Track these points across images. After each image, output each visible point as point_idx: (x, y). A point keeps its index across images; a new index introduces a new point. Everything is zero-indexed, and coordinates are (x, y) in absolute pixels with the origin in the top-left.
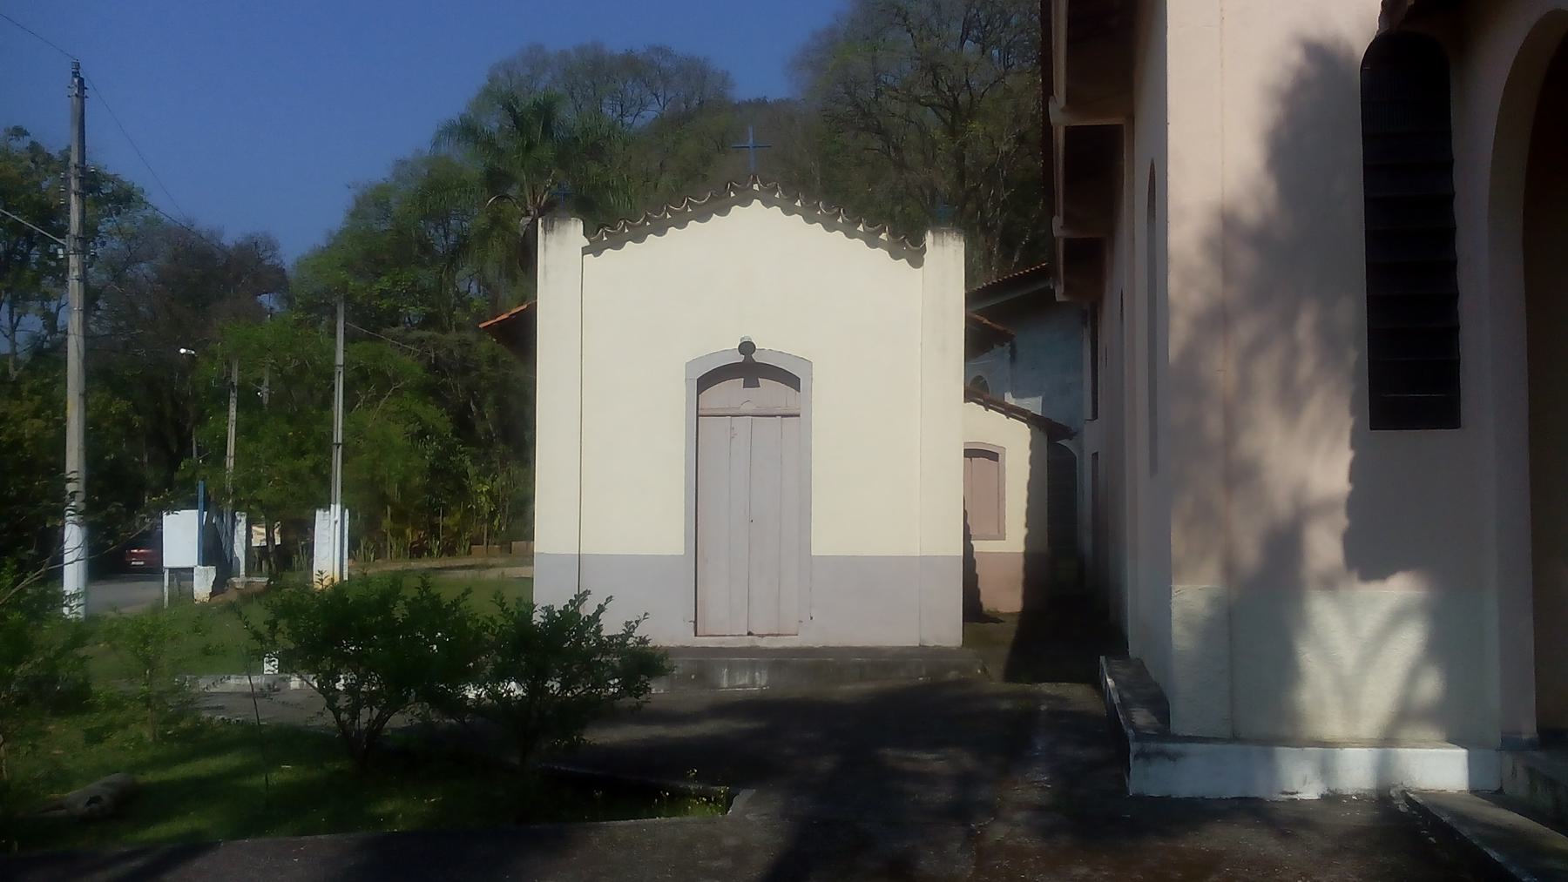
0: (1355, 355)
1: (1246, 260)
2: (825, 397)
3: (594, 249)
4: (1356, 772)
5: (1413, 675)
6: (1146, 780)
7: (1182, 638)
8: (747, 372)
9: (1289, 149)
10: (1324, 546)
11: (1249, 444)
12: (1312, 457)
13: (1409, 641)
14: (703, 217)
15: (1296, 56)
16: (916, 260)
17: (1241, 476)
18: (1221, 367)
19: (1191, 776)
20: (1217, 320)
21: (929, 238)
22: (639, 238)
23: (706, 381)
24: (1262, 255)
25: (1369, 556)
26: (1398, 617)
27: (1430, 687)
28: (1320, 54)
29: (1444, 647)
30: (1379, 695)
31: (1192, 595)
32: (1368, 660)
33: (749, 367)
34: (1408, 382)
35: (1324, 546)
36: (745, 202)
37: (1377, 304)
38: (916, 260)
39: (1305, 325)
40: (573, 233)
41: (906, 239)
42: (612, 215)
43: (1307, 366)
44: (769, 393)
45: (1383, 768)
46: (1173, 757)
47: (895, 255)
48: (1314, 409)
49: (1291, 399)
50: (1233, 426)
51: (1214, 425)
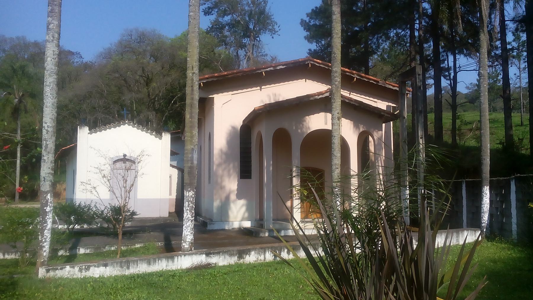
0: (238, 169)
1: (224, 156)
2: (142, 168)
3: (90, 133)
4: (236, 225)
5: (244, 214)
6: (209, 227)
7: (215, 210)
8: (126, 162)
9: (230, 143)
10: (233, 197)
11: (224, 184)
12: (232, 184)
13: (244, 209)
14: (115, 127)
15: (230, 128)
16: (161, 139)
17: (222, 188)
18: (220, 172)
19: (216, 227)
20: (219, 165)
21: (163, 134)
22: (100, 131)
23: (115, 162)
24: (227, 156)
25: (239, 196)
26: (243, 205)
27: (246, 215)
28: (234, 128)
29: (249, 209)
30: (240, 216)
31: (216, 204)
32: (238, 212)
33: (124, 159)
34: (245, 172)
35: (233, 197)
36: (124, 124)
37: (241, 162)
38: (161, 139)
39: (231, 165)
40: (86, 129)
41: (158, 133)
42: (95, 125)
43: (232, 171)
44: (128, 164)
45: (240, 224)
46: (214, 224)
47: (156, 137)
48: (232, 177)
49: (229, 176)
50: (222, 181)
51: (219, 180)
